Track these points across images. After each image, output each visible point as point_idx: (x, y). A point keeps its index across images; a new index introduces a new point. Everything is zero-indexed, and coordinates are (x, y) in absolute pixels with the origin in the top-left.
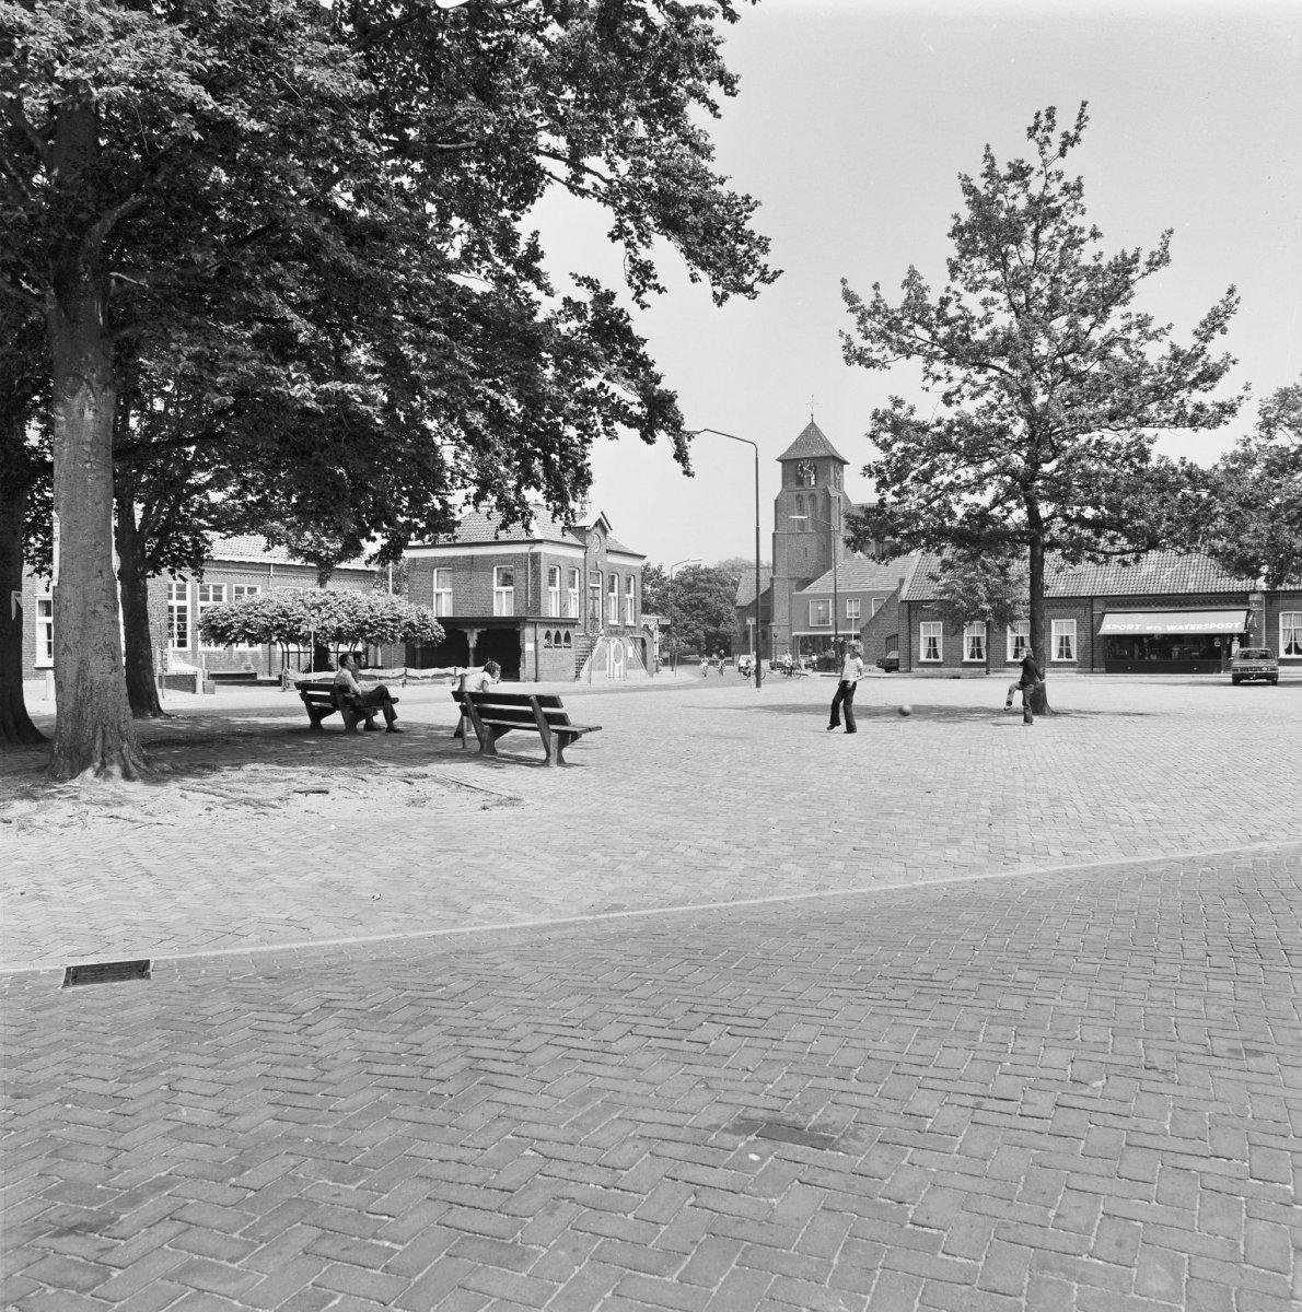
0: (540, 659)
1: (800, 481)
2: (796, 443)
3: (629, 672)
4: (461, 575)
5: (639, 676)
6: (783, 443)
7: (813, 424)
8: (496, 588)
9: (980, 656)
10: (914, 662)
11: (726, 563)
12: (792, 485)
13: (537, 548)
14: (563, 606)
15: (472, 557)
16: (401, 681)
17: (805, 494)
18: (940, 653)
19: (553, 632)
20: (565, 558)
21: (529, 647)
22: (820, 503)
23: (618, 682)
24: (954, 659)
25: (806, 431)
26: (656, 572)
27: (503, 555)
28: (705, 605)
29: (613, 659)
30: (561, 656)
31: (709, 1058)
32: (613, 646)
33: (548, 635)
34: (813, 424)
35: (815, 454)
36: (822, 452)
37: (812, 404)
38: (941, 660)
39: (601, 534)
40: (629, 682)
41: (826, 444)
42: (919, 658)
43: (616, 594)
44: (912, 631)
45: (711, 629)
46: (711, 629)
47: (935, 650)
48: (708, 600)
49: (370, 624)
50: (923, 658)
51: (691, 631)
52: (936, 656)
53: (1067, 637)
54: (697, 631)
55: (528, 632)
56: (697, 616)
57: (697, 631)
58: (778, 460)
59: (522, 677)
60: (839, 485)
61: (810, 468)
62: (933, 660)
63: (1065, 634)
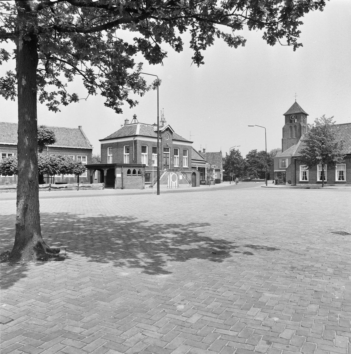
0: (124, 180)
1: (291, 122)
2: (290, 109)
3: (179, 185)
4: (115, 149)
5: (188, 186)
6: (286, 109)
7: (296, 103)
8: (125, 154)
9: (343, 179)
10: (297, 182)
11: (274, 150)
12: (288, 123)
13: (136, 138)
14: (181, 162)
15: (118, 143)
16: (47, 189)
17: (293, 126)
18: (308, 178)
19: (132, 170)
20: (150, 142)
21: (118, 175)
22: (298, 128)
23: (174, 189)
24: (313, 180)
25: (294, 105)
26: (236, 152)
27: (126, 141)
28: (258, 162)
29: (171, 180)
30: (137, 179)
31: (321, 270)
32: (171, 176)
33: (129, 172)
34: (296, 103)
35: (296, 112)
36: (298, 112)
37: (296, 96)
38: (308, 181)
39: (169, 134)
40: (179, 189)
41: (300, 109)
42: (299, 179)
43: (178, 156)
44: (296, 169)
45: (260, 170)
46: (260, 170)
47: (306, 177)
48: (259, 161)
49: (41, 167)
50: (301, 180)
51: (253, 171)
52: (306, 179)
53: (342, 172)
54: (255, 171)
55: (118, 169)
56: (255, 166)
57: (255, 171)
58: (284, 115)
59: (115, 187)
60: (305, 122)
61: (294, 117)
62: (305, 180)
63: (341, 170)
